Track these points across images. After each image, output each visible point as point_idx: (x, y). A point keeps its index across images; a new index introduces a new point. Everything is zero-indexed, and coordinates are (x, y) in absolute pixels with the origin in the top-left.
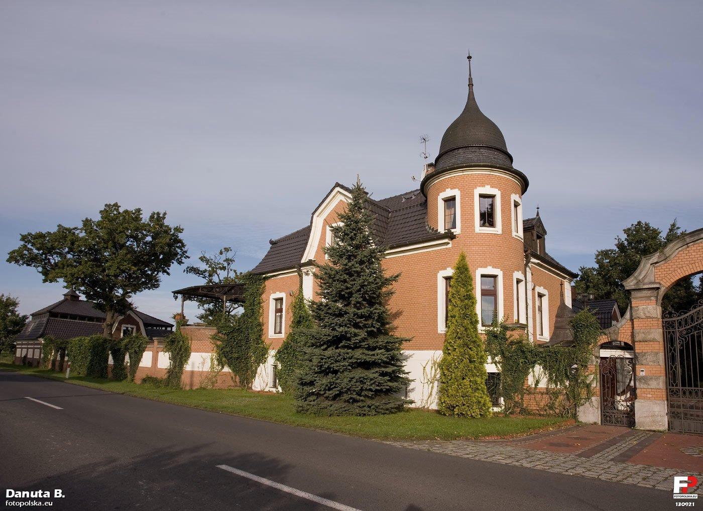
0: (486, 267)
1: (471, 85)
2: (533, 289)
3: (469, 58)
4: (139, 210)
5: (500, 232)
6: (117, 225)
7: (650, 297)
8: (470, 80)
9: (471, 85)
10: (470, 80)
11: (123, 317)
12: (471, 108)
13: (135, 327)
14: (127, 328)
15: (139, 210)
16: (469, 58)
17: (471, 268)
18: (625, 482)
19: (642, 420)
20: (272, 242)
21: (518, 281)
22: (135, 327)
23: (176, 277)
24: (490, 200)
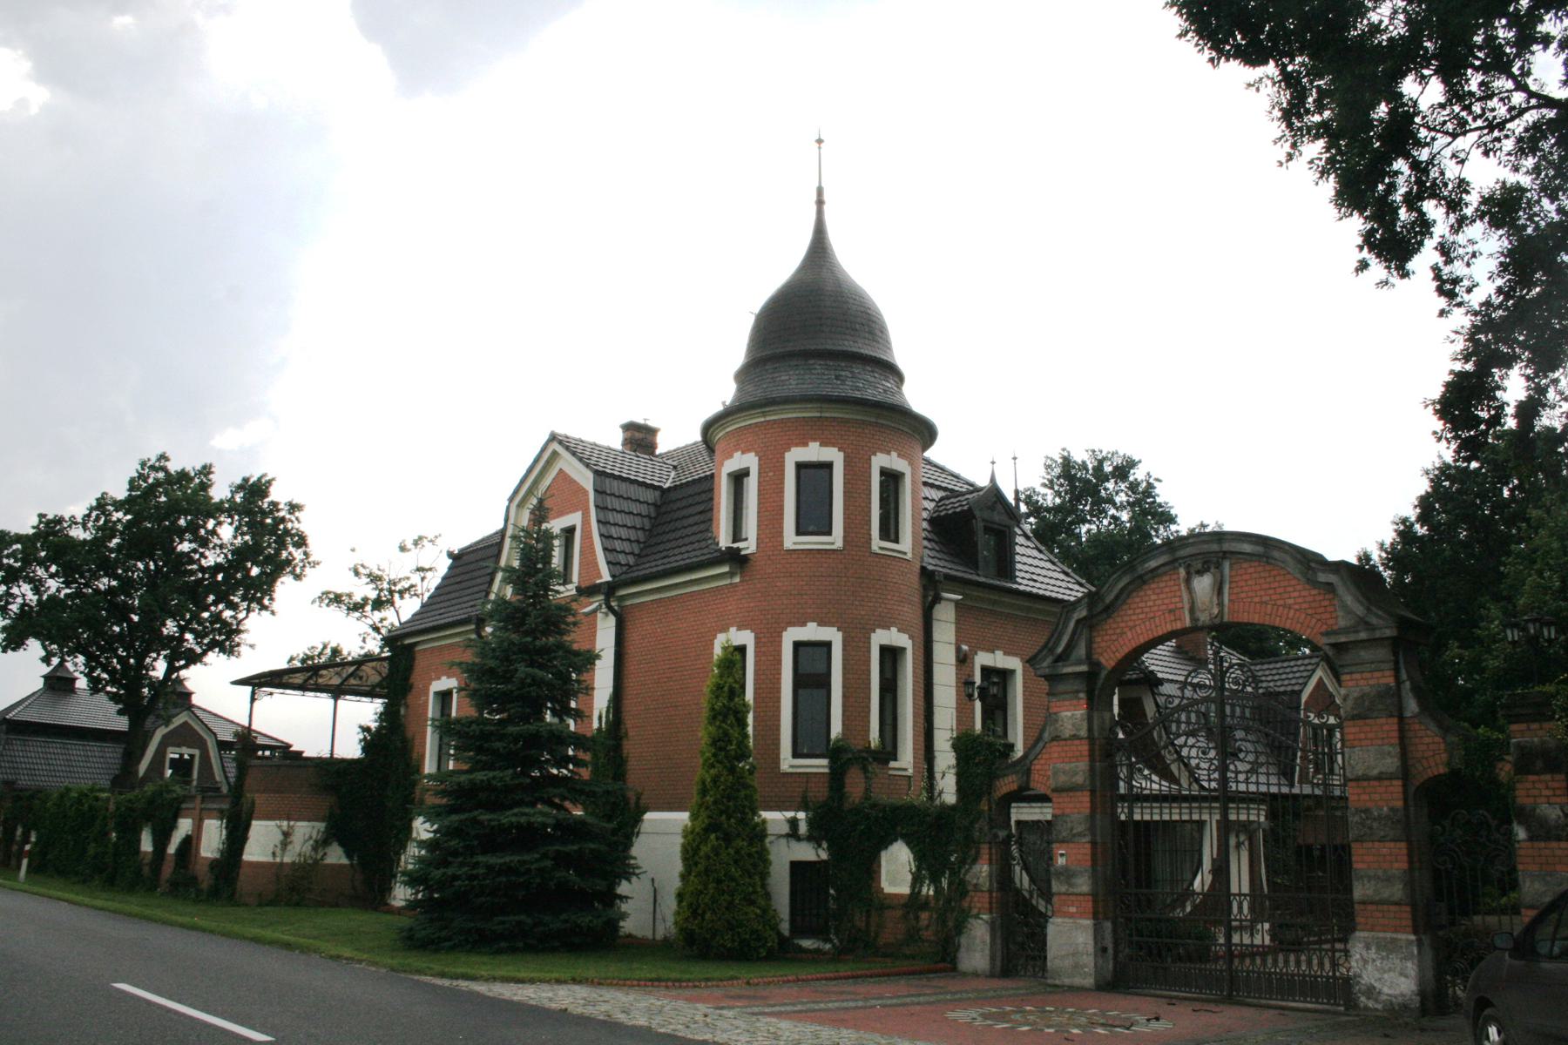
0: (803, 624)
1: (820, 203)
2: (963, 660)
3: (820, 141)
4: (206, 470)
5: (839, 544)
6: (164, 505)
7: (1078, 692)
8: (820, 192)
9: (820, 203)
10: (820, 192)
11: (824, 856)
12: (819, 248)
13: (196, 752)
14: (182, 755)
15: (206, 470)
16: (820, 141)
17: (421, 663)
18: (232, 780)
19: (1057, 962)
20: (450, 555)
21: (891, 655)
22: (196, 752)
23: (285, 626)
24: (823, 472)
